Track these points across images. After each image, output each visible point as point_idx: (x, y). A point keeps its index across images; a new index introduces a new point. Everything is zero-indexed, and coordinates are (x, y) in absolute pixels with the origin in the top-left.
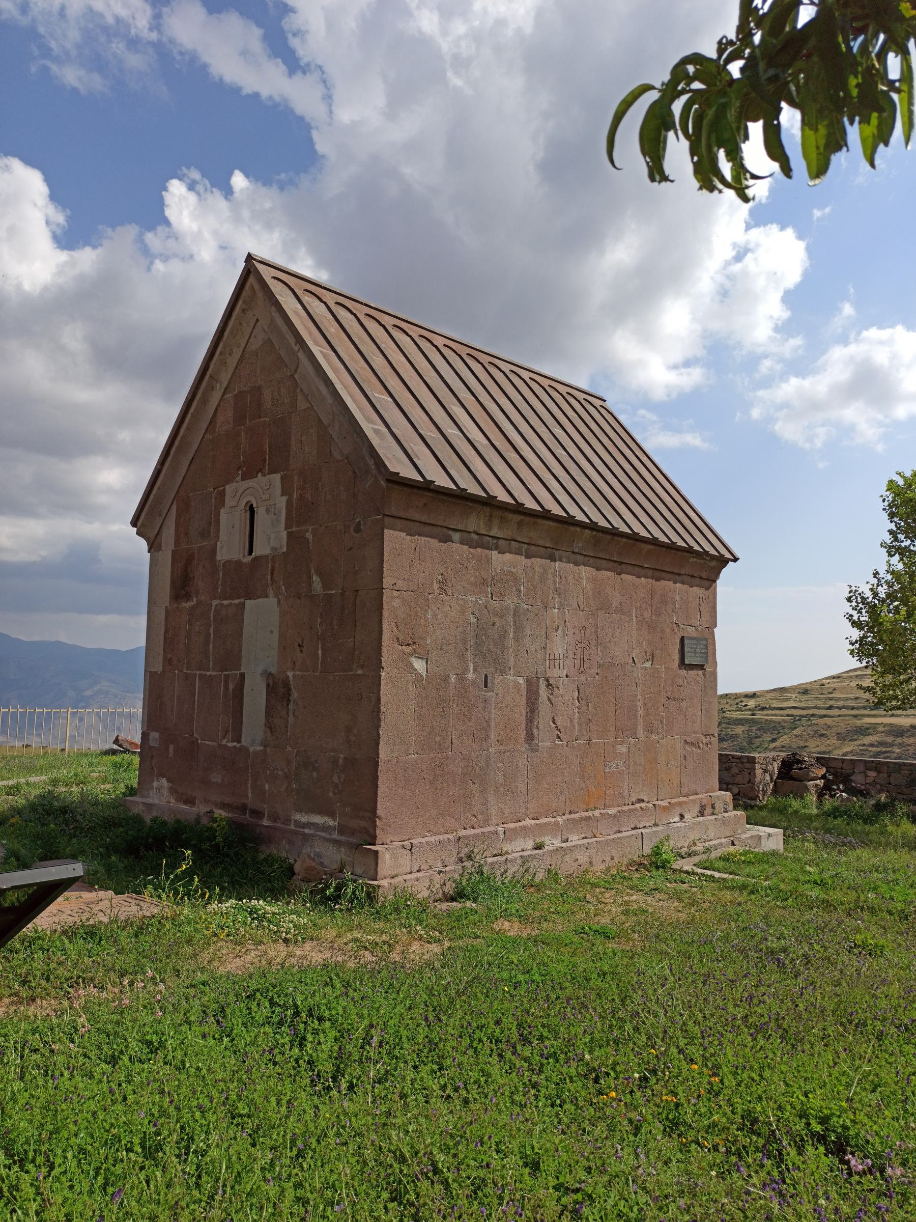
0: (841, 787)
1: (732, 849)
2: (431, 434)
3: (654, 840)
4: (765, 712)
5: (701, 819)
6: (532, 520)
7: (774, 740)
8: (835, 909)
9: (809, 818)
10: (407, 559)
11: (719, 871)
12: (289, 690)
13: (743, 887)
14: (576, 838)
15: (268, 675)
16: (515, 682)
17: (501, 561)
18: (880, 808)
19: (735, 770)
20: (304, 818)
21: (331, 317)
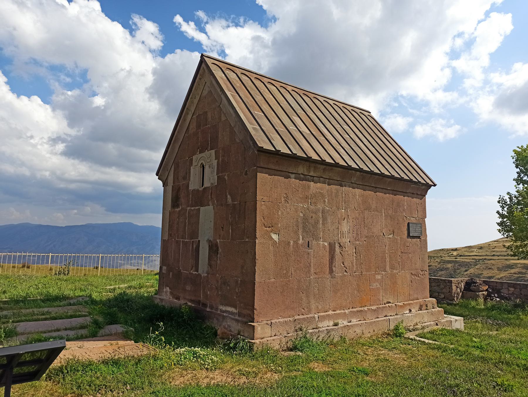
0: (496, 295)
1: (436, 327)
2: (281, 129)
3: (396, 322)
4: (462, 257)
5: (420, 312)
6: (330, 168)
7: (466, 271)
8: (488, 362)
9: (481, 310)
10: (268, 187)
11: (428, 339)
12: (218, 248)
13: (439, 348)
14: (355, 320)
15: (209, 241)
16: (323, 244)
17: (314, 187)
18: (516, 306)
19: (442, 286)
20: (224, 308)
21: (238, 79)
